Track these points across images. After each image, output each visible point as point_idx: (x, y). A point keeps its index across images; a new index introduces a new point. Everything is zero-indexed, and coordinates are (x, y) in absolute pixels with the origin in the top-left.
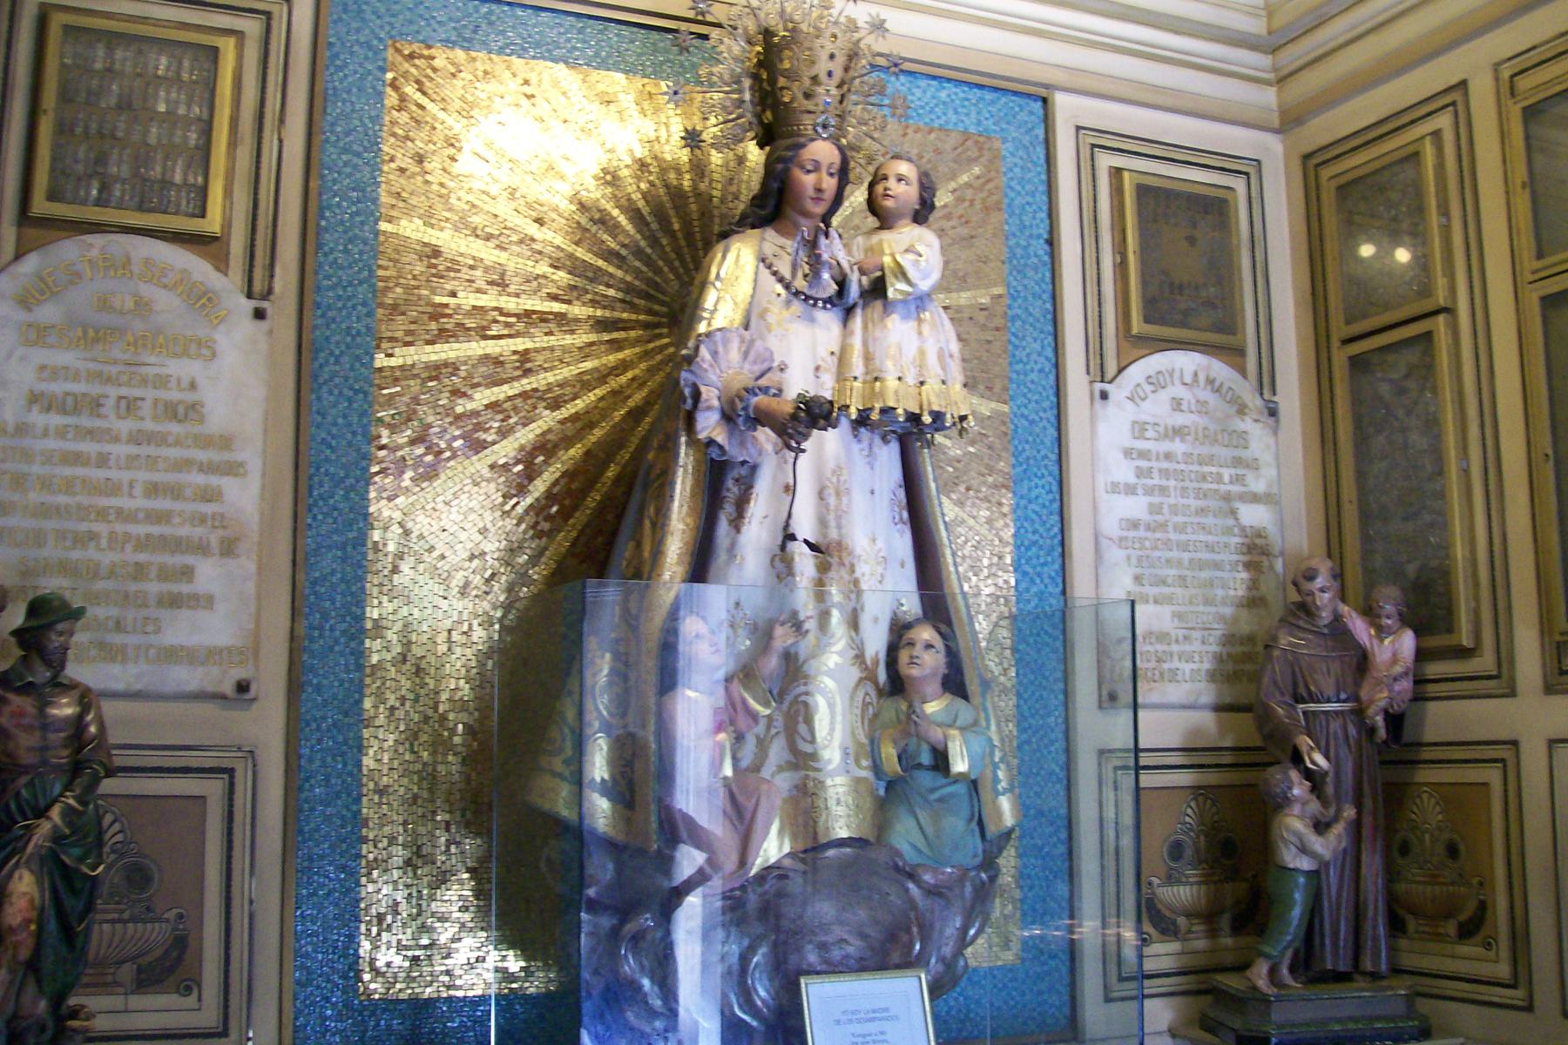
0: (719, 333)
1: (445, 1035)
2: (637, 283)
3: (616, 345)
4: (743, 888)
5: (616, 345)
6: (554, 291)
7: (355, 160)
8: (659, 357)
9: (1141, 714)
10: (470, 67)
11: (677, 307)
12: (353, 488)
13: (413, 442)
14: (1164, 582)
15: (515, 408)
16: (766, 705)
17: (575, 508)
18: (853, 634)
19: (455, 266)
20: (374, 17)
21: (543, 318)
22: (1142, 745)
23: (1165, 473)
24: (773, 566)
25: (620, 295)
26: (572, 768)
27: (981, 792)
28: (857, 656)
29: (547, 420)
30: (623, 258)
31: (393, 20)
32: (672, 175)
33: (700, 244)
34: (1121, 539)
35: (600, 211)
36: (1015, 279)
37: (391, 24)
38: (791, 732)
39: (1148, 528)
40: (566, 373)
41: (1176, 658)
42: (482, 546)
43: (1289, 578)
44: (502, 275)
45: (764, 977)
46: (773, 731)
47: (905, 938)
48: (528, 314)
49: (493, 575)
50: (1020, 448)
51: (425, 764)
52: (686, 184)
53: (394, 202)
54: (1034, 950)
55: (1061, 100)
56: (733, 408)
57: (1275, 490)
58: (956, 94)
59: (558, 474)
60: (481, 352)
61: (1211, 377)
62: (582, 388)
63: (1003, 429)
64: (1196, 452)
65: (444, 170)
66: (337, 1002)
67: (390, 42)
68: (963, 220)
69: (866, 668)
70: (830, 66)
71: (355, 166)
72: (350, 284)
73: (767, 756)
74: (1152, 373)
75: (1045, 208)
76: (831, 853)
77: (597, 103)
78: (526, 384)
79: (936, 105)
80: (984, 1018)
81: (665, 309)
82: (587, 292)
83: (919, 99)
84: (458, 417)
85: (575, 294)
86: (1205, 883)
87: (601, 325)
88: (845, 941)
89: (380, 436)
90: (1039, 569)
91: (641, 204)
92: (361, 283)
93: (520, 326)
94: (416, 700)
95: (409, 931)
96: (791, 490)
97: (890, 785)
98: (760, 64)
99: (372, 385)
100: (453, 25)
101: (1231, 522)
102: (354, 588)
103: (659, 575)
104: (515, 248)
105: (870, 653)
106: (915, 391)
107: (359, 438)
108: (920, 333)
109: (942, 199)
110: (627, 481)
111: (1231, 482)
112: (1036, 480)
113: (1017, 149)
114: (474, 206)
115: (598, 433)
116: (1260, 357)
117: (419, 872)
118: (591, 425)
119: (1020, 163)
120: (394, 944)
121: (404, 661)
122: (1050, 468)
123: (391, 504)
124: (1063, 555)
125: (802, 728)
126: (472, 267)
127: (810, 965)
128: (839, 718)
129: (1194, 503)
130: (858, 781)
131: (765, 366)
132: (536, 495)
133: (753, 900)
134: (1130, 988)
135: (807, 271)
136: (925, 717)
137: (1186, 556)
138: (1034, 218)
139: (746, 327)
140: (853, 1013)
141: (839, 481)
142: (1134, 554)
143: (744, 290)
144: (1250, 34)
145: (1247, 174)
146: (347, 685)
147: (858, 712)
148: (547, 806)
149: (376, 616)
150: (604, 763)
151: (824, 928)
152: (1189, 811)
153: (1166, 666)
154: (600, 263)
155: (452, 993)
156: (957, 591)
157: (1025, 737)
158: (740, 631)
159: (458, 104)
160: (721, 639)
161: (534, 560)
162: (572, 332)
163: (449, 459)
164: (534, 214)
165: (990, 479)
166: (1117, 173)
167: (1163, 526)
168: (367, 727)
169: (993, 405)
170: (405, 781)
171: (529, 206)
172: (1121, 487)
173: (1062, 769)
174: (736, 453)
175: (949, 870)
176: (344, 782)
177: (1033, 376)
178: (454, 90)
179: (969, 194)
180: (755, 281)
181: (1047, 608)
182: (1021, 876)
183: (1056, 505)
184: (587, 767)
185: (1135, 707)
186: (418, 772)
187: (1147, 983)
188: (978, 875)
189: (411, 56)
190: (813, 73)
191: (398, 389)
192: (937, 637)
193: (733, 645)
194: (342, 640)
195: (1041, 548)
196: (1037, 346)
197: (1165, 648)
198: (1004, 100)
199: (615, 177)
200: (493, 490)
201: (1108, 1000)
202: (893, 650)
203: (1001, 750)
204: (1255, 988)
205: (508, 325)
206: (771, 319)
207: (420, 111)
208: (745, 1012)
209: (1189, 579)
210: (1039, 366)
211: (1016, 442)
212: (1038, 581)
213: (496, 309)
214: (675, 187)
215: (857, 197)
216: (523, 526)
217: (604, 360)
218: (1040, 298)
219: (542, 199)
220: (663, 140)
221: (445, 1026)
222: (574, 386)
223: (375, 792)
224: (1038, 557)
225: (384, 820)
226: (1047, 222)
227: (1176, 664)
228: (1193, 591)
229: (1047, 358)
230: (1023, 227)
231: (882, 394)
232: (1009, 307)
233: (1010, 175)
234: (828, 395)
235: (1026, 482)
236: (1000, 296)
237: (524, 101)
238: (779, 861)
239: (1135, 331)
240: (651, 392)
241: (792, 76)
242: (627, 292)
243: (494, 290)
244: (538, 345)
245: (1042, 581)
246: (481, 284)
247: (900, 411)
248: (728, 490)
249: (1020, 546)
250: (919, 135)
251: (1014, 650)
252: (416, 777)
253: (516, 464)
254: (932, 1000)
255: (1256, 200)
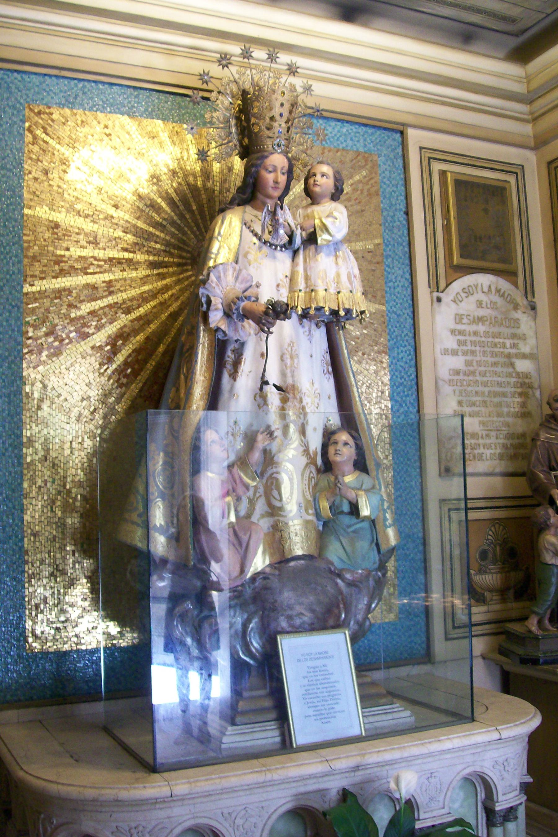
0: (221, 266)
1: (76, 671)
2: (172, 240)
3: (162, 276)
4: (242, 585)
5: (162, 276)
6: (125, 246)
7: (8, 173)
8: (186, 283)
9: (468, 479)
10: (73, 118)
11: (196, 254)
12: (13, 362)
13: (47, 335)
14: (474, 404)
15: (105, 314)
16: (254, 479)
17: (141, 370)
18: (303, 438)
19: (67, 234)
20: (16, 91)
21: (119, 262)
22: (469, 496)
23: (473, 343)
24: (255, 400)
25: (163, 248)
26: (143, 519)
27: (377, 527)
28: (305, 451)
29: (123, 320)
30: (165, 227)
31: (28, 92)
32: (191, 179)
33: (208, 218)
34: (450, 381)
35: (150, 200)
36: (387, 234)
37: (26, 95)
38: (268, 495)
39: (465, 374)
40: (133, 293)
41: (482, 447)
42: (88, 393)
43: (545, 399)
44: (96, 238)
45: (257, 637)
46: (258, 495)
47: (336, 611)
48: (111, 260)
49: (95, 410)
50: (392, 330)
51: (59, 518)
52: (199, 183)
53: (32, 197)
54: (404, 611)
55: (411, 133)
56: (231, 310)
57: (535, 351)
58: (352, 129)
59: (130, 351)
60: (84, 282)
61: (499, 288)
62: (143, 301)
63: (382, 319)
64: (491, 331)
65: (60, 178)
66: (14, 655)
67: (26, 105)
68: (357, 201)
69: (310, 457)
70: (281, 110)
71: (8, 177)
72: (8, 245)
73: (254, 509)
74: (466, 286)
75: (403, 194)
76: (292, 564)
77: (147, 138)
78: (110, 300)
79: (340, 136)
80: (378, 652)
81: (189, 255)
82: (144, 246)
83: (331, 133)
84: (72, 320)
85: (137, 247)
86: (501, 573)
87: (153, 265)
88: (302, 614)
89: (28, 332)
90: (404, 398)
91: (174, 195)
92: (14, 244)
93: (107, 266)
94: (53, 482)
95: (53, 613)
96: (264, 356)
97: (325, 525)
98: (240, 111)
99: (22, 303)
100: (62, 94)
101: (511, 370)
102: (15, 420)
103: (190, 407)
104: (102, 222)
105: (312, 448)
106: (334, 297)
107: (16, 333)
108: (337, 264)
109: (347, 189)
110: (170, 353)
111: (511, 347)
112: (402, 348)
113: (387, 161)
114: (77, 198)
115: (153, 327)
116: (525, 277)
117: (58, 579)
118: (149, 323)
119: (389, 168)
120: (45, 621)
121: (46, 460)
122: (409, 341)
123: (35, 371)
124: (418, 390)
125: (275, 493)
126: (78, 234)
127: (282, 628)
128: (295, 486)
129: (490, 360)
130: (307, 522)
131: (248, 285)
132: (118, 363)
133: (249, 592)
134: (462, 632)
135: (271, 229)
136: (345, 484)
137: (486, 390)
138: (397, 199)
139: (237, 262)
140: (308, 655)
141: (292, 350)
142: (458, 389)
143: (234, 241)
144: (520, 93)
145: (517, 173)
146: (13, 475)
147: (307, 483)
148: (129, 541)
149: (28, 435)
150: (161, 515)
151: (290, 607)
152: (491, 533)
153: (476, 452)
154: (151, 229)
155: (79, 647)
156: (361, 411)
157: (398, 493)
158: (237, 438)
159: (67, 140)
160: (225, 442)
161: (118, 400)
162: (136, 269)
163: (68, 344)
164: (112, 202)
165: (376, 348)
166: (443, 174)
167: (473, 373)
168: (26, 498)
169: (377, 306)
170: (48, 528)
171: (110, 198)
172: (450, 351)
173: (419, 510)
174: (232, 335)
175: (360, 571)
176: (13, 529)
177: (399, 289)
178: (64, 132)
179: (360, 186)
180: (241, 236)
181: (409, 421)
182: (397, 571)
183: (413, 362)
184: (151, 519)
185: (465, 475)
186: (56, 523)
187: (474, 628)
188: (376, 574)
189: (39, 113)
190: (271, 115)
191: (37, 304)
192: (351, 438)
193: (234, 445)
194: (10, 449)
195: (405, 387)
196: (400, 272)
197: (476, 441)
198: (378, 133)
199: (159, 180)
200: (94, 361)
201: (447, 639)
202: (325, 447)
203: (387, 502)
204: (530, 631)
205: (99, 266)
206: (251, 257)
207: (45, 144)
208: (246, 656)
209: (488, 403)
210: (402, 284)
211: (390, 327)
212: (404, 405)
213: (92, 257)
214: (193, 185)
215: (298, 188)
216: (112, 381)
217: (155, 285)
218: (402, 245)
219: (117, 194)
220: (185, 158)
221: (76, 665)
222: (138, 300)
223: (31, 534)
224: (404, 392)
225: (37, 551)
226: (405, 202)
227: (482, 450)
228: (491, 409)
229: (406, 279)
230: (391, 205)
231: (316, 299)
232: (384, 250)
233: (383, 175)
234: (285, 300)
235: (396, 349)
236: (379, 244)
237: (105, 138)
238: (263, 569)
239: (455, 262)
240: (182, 303)
241: (259, 117)
242: (166, 246)
243: (91, 247)
244: (117, 277)
245: (406, 405)
246: (83, 243)
247: (326, 309)
248: (229, 357)
249: (393, 384)
250: (331, 154)
251: (391, 444)
252: (54, 526)
253: (106, 346)
254: (352, 645)
255: (522, 188)
